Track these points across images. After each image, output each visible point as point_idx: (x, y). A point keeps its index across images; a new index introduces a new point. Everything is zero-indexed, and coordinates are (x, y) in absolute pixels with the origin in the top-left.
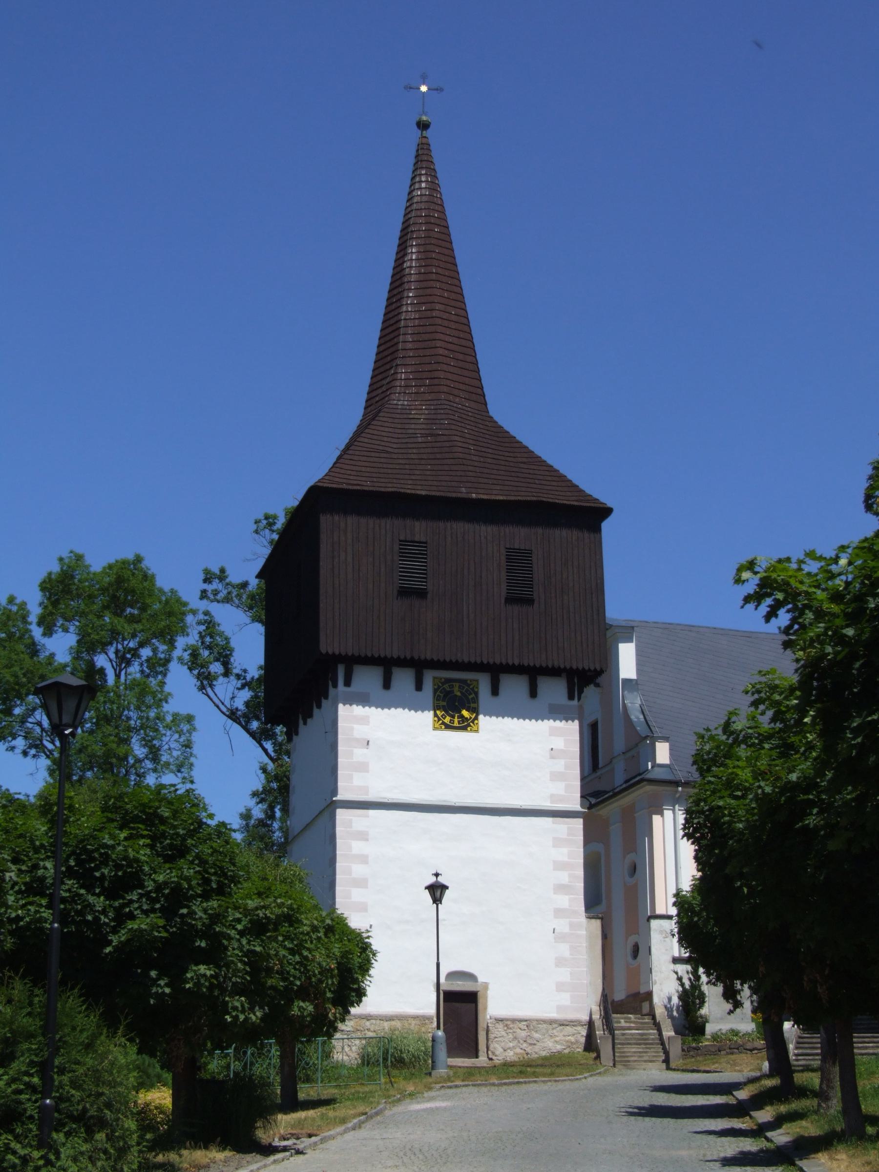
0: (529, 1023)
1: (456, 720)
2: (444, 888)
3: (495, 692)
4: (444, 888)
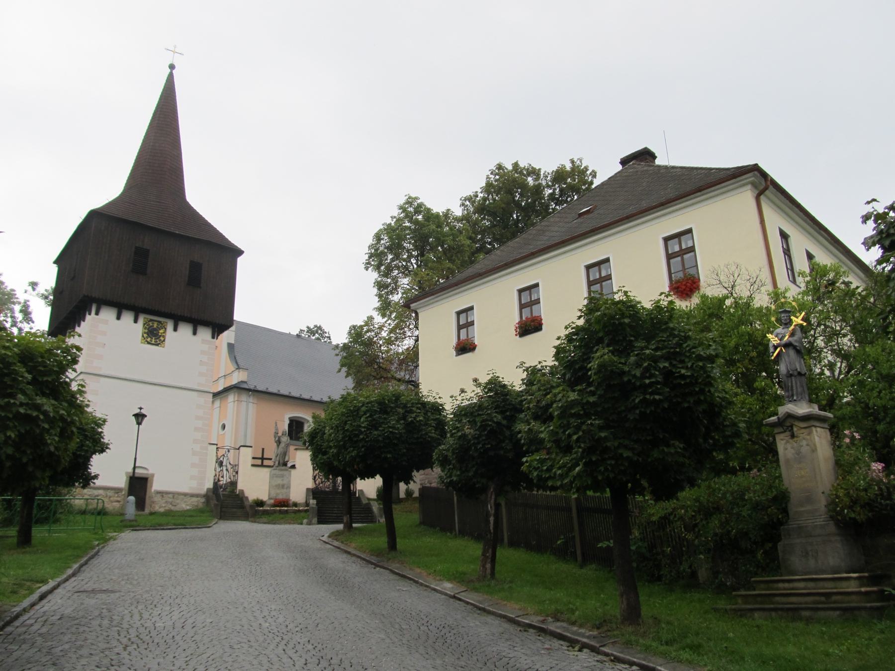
0: (174, 494)
2: (144, 416)
3: (175, 329)
4: (144, 416)
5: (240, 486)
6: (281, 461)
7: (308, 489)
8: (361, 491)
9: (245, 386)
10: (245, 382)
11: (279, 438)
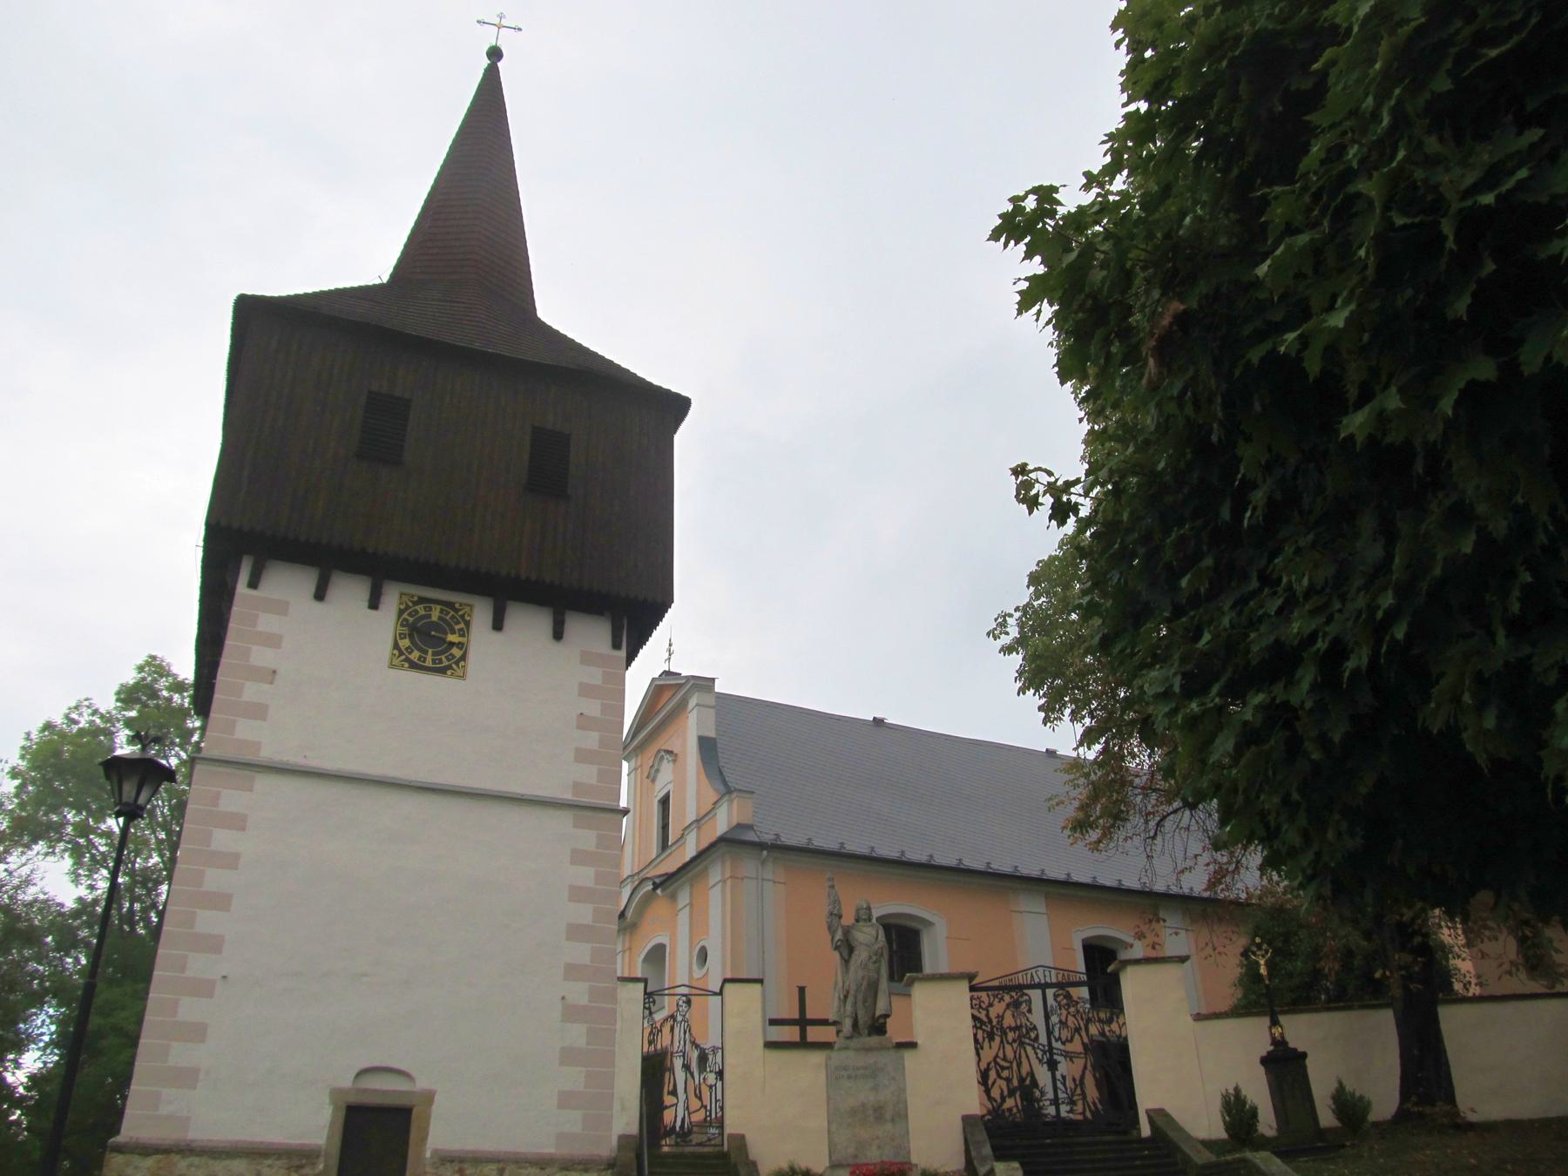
1: (429, 657)
3: (498, 625)
5: (1348, 1088)
6: (863, 1019)
7: (966, 1119)
8: (1157, 1116)
9: (750, 836)
10: (750, 827)
11: (847, 931)
